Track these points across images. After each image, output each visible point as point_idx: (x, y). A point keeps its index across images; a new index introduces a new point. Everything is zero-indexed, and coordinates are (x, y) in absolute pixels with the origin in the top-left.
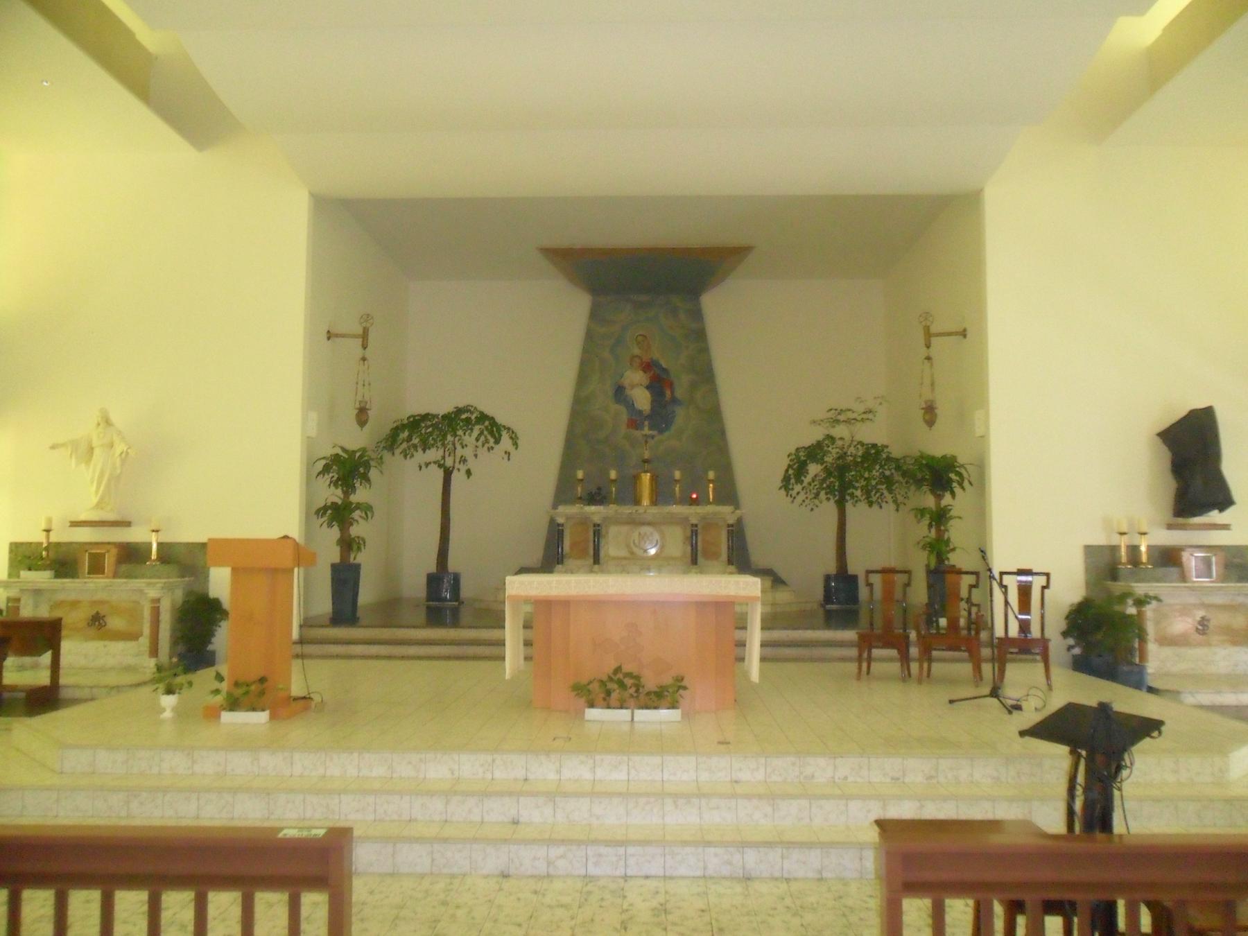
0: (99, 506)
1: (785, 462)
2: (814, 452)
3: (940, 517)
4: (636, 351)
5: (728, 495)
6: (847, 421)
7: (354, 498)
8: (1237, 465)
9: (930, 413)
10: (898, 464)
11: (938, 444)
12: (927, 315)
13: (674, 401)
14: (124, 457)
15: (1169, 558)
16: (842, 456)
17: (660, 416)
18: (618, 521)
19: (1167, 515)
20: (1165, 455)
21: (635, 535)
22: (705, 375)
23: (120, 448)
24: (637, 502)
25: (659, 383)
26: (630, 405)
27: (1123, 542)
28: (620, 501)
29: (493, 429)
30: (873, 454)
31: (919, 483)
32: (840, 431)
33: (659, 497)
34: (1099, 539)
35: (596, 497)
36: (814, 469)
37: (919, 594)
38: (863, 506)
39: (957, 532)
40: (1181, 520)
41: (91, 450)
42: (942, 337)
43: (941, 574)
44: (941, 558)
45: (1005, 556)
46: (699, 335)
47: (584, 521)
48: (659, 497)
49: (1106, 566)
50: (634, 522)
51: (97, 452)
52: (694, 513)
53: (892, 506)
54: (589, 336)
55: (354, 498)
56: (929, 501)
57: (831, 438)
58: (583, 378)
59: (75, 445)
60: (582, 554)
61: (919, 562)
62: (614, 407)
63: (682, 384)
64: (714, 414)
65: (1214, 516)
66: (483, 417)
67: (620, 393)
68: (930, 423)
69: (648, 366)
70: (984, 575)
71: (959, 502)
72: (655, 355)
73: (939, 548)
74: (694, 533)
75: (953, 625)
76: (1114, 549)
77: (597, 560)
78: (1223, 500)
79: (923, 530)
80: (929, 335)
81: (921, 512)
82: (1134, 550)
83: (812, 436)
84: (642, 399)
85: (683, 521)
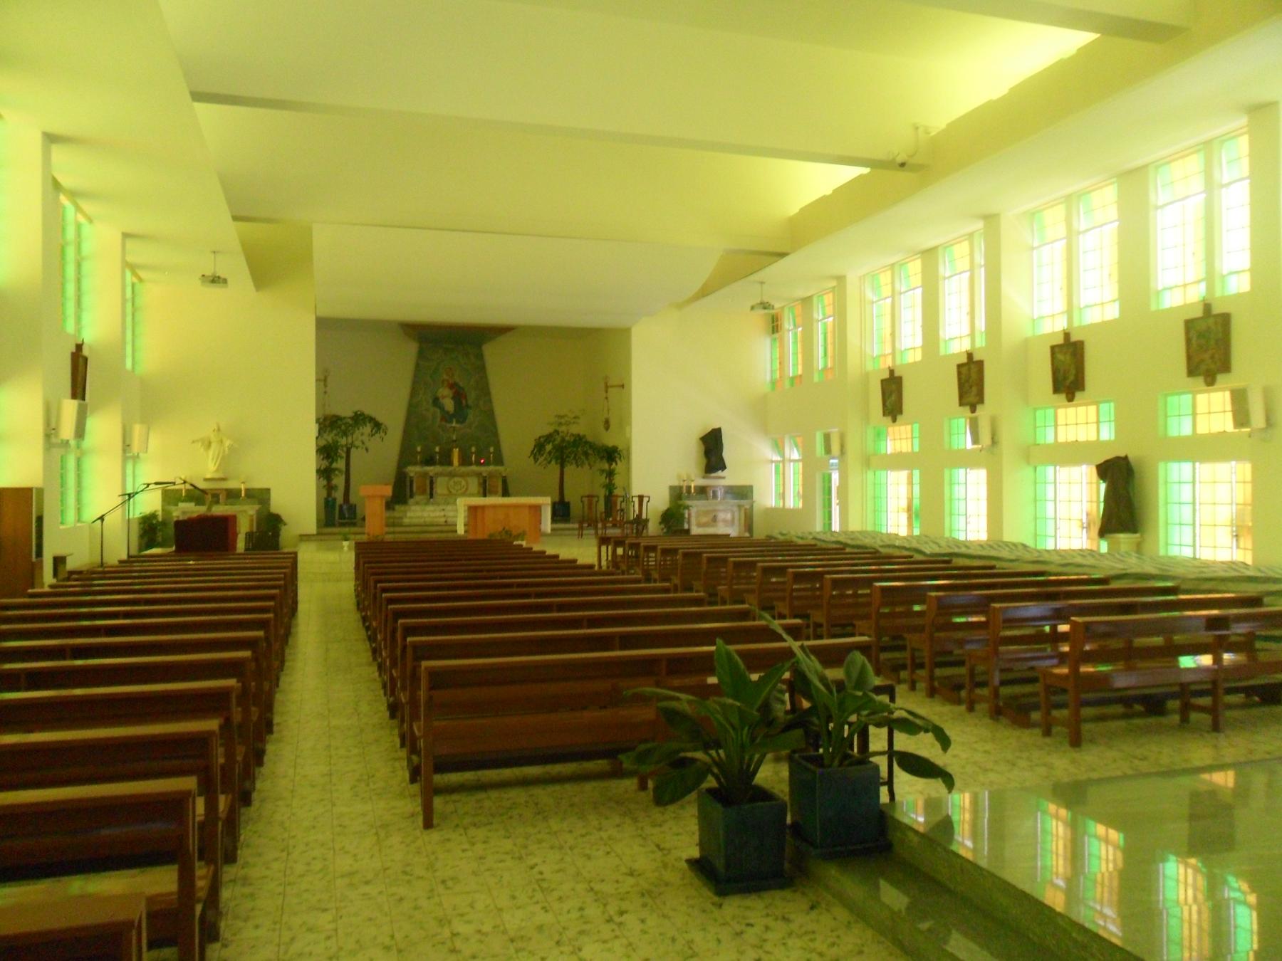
0: (217, 470)
1: (533, 444)
2: (549, 438)
3: (611, 474)
4: (445, 377)
5: (499, 460)
6: (806, 933)
7: (334, 465)
8: (729, 453)
9: (607, 424)
10: (592, 446)
11: (609, 440)
12: (606, 378)
13: (467, 406)
14: (231, 448)
15: (702, 491)
16: (563, 440)
17: (460, 412)
18: (441, 474)
19: (702, 473)
20: (702, 448)
21: (452, 483)
22: (485, 391)
23: (227, 443)
24: (450, 464)
25: (459, 396)
26: (442, 408)
27: (685, 484)
28: (441, 464)
29: (377, 426)
30: (579, 440)
31: (602, 458)
32: (563, 428)
33: (465, 461)
34: (676, 483)
35: (430, 461)
36: (549, 447)
37: (601, 506)
38: (574, 466)
39: (618, 480)
40: (219, 510)
41: (210, 443)
42: (611, 386)
43: (610, 499)
44: (611, 492)
45: (636, 490)
46: (482, 369)
47: (425, 474)
48: (465, 461)
49: (679, 494)
50: (451, 475)
51: (213, 445)
52: (485, 470)
53: (587, 467)
54: (417, 365)
55: (334, 465)
56: (606, 466)
57: (557, 432)
58: (414, 393)
59: (202, 440)
60: (423, 492)
61: (602, 493)
62: (432, 409)
63: (472, 397)
64: (490, 414)
65: (720, 473)
66: (372, 419)
67: (436, 401)
68: (607, 428)
69: (452, 386)
70: (627, 499)
71: (619, 467)
72: (457, 379)
73: (610, 487)
74: (485, 482)
75: (615, 519)
76: (681, 487)
77: (431, 496)
78: (723, 467)
79: (603, 479)
80: (607, 387)
81: (603, 471)
82: (689, 488)
83: (547, 430)
84: (449, 405)
85: (479, 474)
